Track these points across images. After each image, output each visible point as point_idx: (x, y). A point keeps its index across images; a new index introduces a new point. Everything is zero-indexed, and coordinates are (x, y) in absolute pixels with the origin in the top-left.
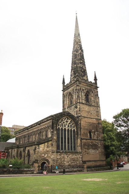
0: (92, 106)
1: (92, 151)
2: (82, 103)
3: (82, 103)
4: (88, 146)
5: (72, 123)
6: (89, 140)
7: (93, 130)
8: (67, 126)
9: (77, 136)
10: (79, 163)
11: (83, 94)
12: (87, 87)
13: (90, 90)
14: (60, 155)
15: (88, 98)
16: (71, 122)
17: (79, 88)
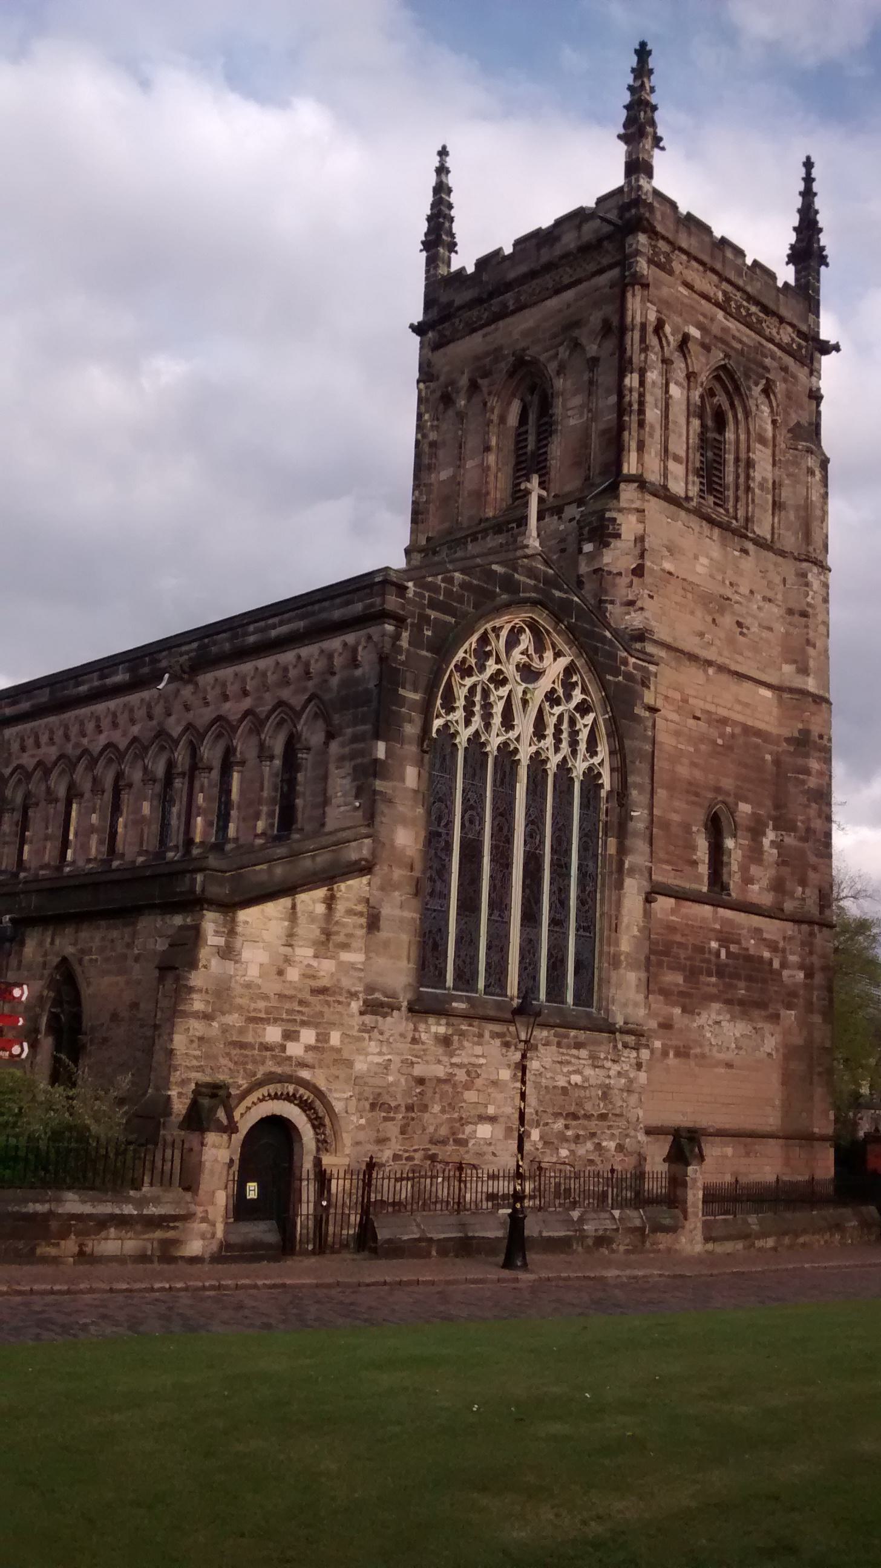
0: (750, 546)
1: (721, 1029)
2: (663, 494)
3: (663, 494)
4: (692, 974)
5: (578, 696)
6: (707, 909)
7: (745, 808)
8: (524, 725)
9: (612, 849)
10: (620, 1148)
11: (675, 391)
12: (720, 315)
13: (755, 367)
14: (445, 1041)
15: (718, 448)
16: (568, 687)
17: (652, 317)
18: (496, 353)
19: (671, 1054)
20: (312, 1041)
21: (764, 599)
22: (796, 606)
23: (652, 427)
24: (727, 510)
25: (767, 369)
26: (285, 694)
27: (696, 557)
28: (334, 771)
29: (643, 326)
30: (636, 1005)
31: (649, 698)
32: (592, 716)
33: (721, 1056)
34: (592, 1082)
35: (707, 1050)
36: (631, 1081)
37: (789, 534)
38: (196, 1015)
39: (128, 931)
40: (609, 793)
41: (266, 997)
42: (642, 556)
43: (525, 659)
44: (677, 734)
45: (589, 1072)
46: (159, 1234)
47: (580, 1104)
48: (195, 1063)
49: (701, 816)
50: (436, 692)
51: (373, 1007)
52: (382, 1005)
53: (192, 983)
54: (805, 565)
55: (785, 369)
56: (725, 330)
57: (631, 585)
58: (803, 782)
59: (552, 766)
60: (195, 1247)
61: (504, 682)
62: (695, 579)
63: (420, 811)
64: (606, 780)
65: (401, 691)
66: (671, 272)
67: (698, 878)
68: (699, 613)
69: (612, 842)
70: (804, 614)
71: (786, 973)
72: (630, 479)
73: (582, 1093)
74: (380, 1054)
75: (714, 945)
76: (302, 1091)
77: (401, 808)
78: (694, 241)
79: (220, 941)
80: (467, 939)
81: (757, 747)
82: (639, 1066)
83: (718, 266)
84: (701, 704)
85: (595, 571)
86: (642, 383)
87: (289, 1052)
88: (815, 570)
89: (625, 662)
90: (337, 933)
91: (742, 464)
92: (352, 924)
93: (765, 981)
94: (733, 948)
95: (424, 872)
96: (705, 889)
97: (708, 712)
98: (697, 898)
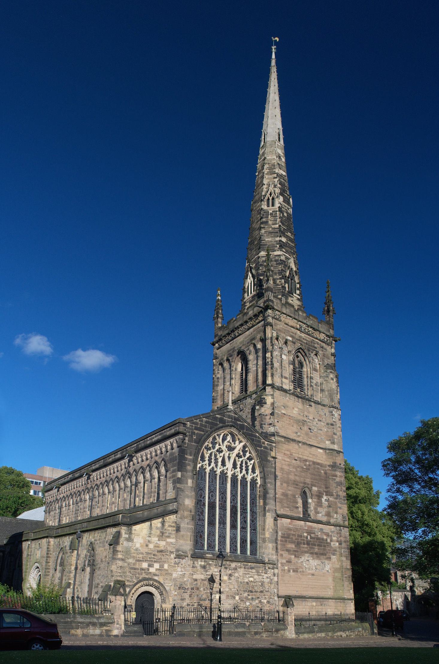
0: (312, 404)
1: (309, 562)
4: (298, 544)
5: (248, 455)
7: (315, 489)
8: (229, 465)
9: (262, 504)
11: (284, 357)
12: (298, 332)
14: (204, 567)
15: (301, 373)
17: (275, 335)
18: (233, 349)
19: (291, 571)
20: (158, 567)
21: (318, 420)
22: (330, 422)
23: (276, 369)
24: (305, 393)
25: (316, 348)
26: (157, 458)
27: (293, 408)
28: (169, 482)
29: (271, 338)
30: (272, 554)
31: (273, 454)
32: (253, 461)
33: (310, 572)
34: (257, 580)
35: (304, 570)
36: (271, 580)
37: (326, 399)
38: (119, 559)
39: (104, 534)
40: (260, 485)
41: (142, 554)
42: (273, 409)
43: (229, 444)
44: (289, 465)
45: (256, 577)
46: (105, 628)
47: (253, 587)
48: (119, 574)
49: (299, 492)
50: (198, 455)
51: (178, 556)
52: (182, 555)
53: (118, 549)
54: (332, 409)
55: (322, 347)
56: (300, 337)
57: (270, 418)
58: (335, 479)
59: (239, 478)
60: (115, 632)
61: (222, 451)
62: (294, 416)
63: (193, 493)
64: (259, 481)
65: (186, 456)
66: (280, 321)
67: (299, 513)
68: (295, 426)
69: (262, 501)
70: (332, 425)
71: (332, 543)
72: (269, 385)
73: (254, 584)
74: (181, 571)
75: (305, 534)
76: (155, 583)
77: (186, 493)
78: (288, 310)
79: (127, 536)
80: (211, 534)
81: (318, 468)
82: (274, 575)
83: (297, 317)
84: (297, 455)
85: (260, 415)
86: (272, 355)
87: (150, 571)
88: (335, 410)
89: (264, 443)
90: (166, 533)
91: (309, 378)
92: (170, 530)
93: (325, 546)
94: (313, 535)
95: (195, 513)
96: (302, 516)
97: (300, 458)
98: (299, 519)
